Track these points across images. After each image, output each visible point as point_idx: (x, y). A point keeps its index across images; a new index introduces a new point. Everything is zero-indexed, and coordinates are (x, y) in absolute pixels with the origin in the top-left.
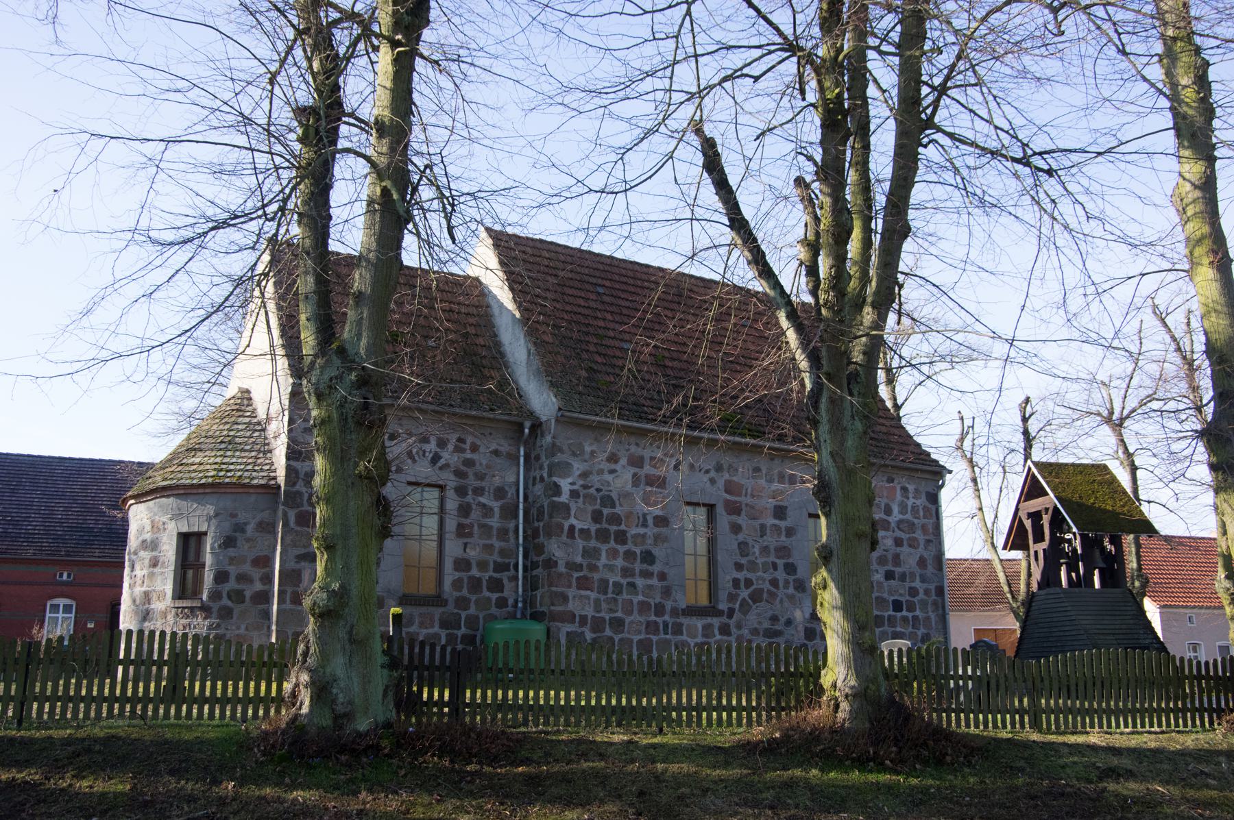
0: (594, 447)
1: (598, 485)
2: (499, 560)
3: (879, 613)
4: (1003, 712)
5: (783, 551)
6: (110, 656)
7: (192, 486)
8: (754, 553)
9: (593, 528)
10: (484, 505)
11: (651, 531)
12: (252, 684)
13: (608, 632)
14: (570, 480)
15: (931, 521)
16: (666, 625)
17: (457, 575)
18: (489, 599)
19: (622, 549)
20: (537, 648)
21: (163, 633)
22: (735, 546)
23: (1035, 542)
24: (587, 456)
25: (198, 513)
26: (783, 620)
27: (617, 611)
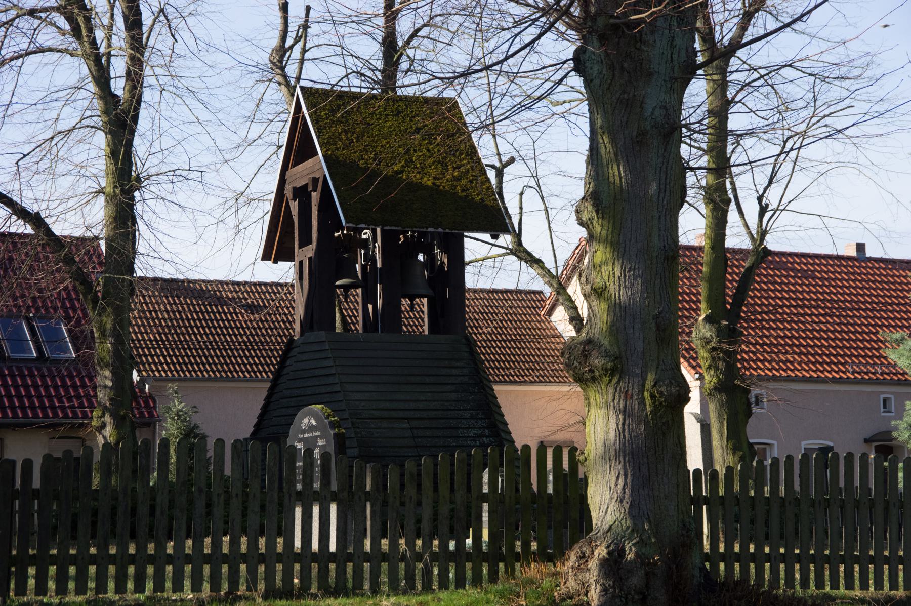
6: (469, 489)
23: (301, 246)
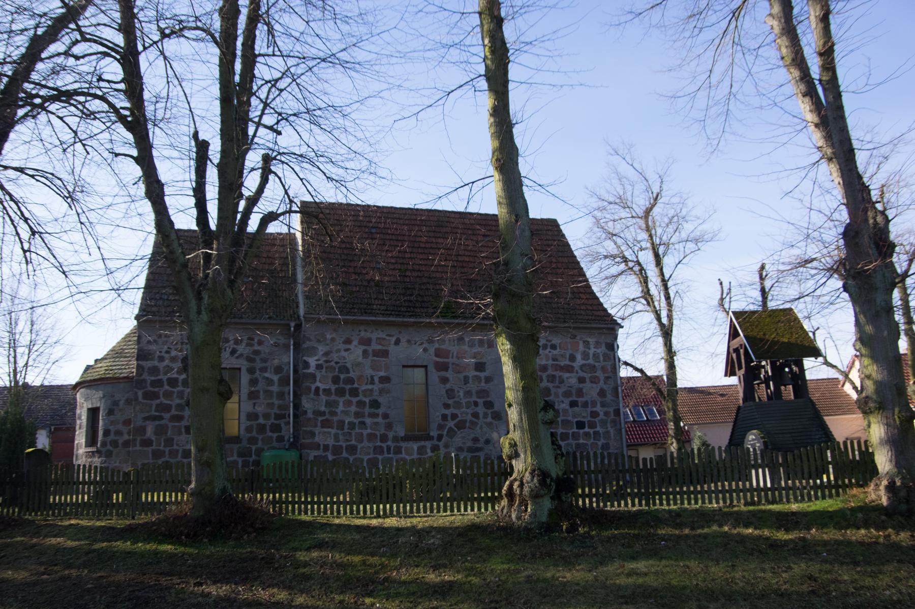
0: (334, 335)
1: (336, 360)
2: (278, 412)
3: (564, 431)
4: (441, 499)
5: (482, 393)
7: (95, 380)
8: (459, 396)
9: (333, 388)
10: (267, 378)
11: (376, 387)
12: (74, 496)
13: (345, 455)
14: (316, 358)
15: (610, 363)
16: (389, 448)
17: (249, 423)
18: (271, 437)
19: (354, 400)
20: (293, 466)
21: (84, 466)
22: (444, 392)
24: (328, 342)
25: (95, 397)
26: (482, 440)
27: (351, 441)
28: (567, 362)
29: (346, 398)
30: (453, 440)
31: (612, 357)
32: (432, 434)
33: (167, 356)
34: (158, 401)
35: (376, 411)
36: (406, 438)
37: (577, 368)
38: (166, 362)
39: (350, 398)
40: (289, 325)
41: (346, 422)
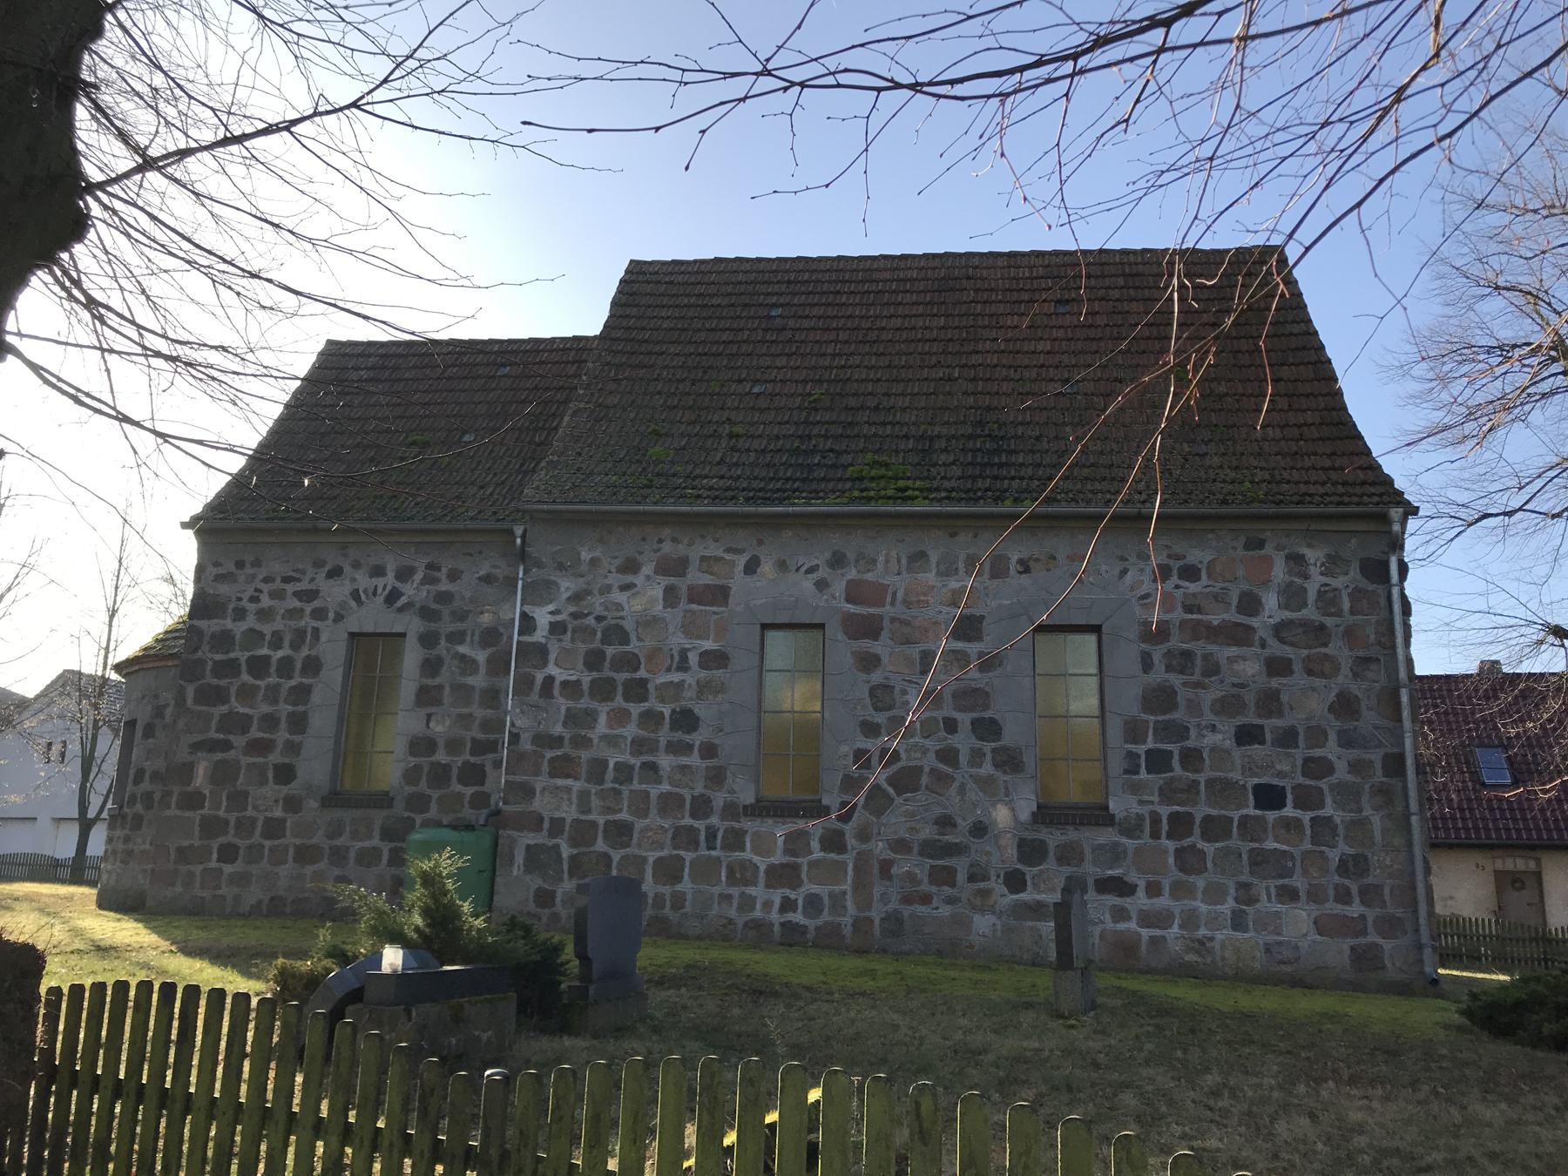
0: (597, 554)
1: (599, 610)
2: (480, 736)
3: (1214, 812)
5: (970, 697)
10: (463, 657)
13: (600, 845)
14: (551, 607)
15: (1374, 619)
16: (711, 834)
17: (413, 761)
18: (460, 796)
19: (635, 709)
24: (584, 568)
26: (964, 824)
27: (620, 810)
28: (1232, 616)
29: (614, 704)
30: (884, 819)
31: (1383, 602)
32: (825, 801)
33: (252, 607)
34: (224, 709)
35: (687, 738)
36: (765, 808)
37: (1262, 633)
38: (251, 622)
39: (624, 705)
40: (511, 533)
41: (611, 765)
